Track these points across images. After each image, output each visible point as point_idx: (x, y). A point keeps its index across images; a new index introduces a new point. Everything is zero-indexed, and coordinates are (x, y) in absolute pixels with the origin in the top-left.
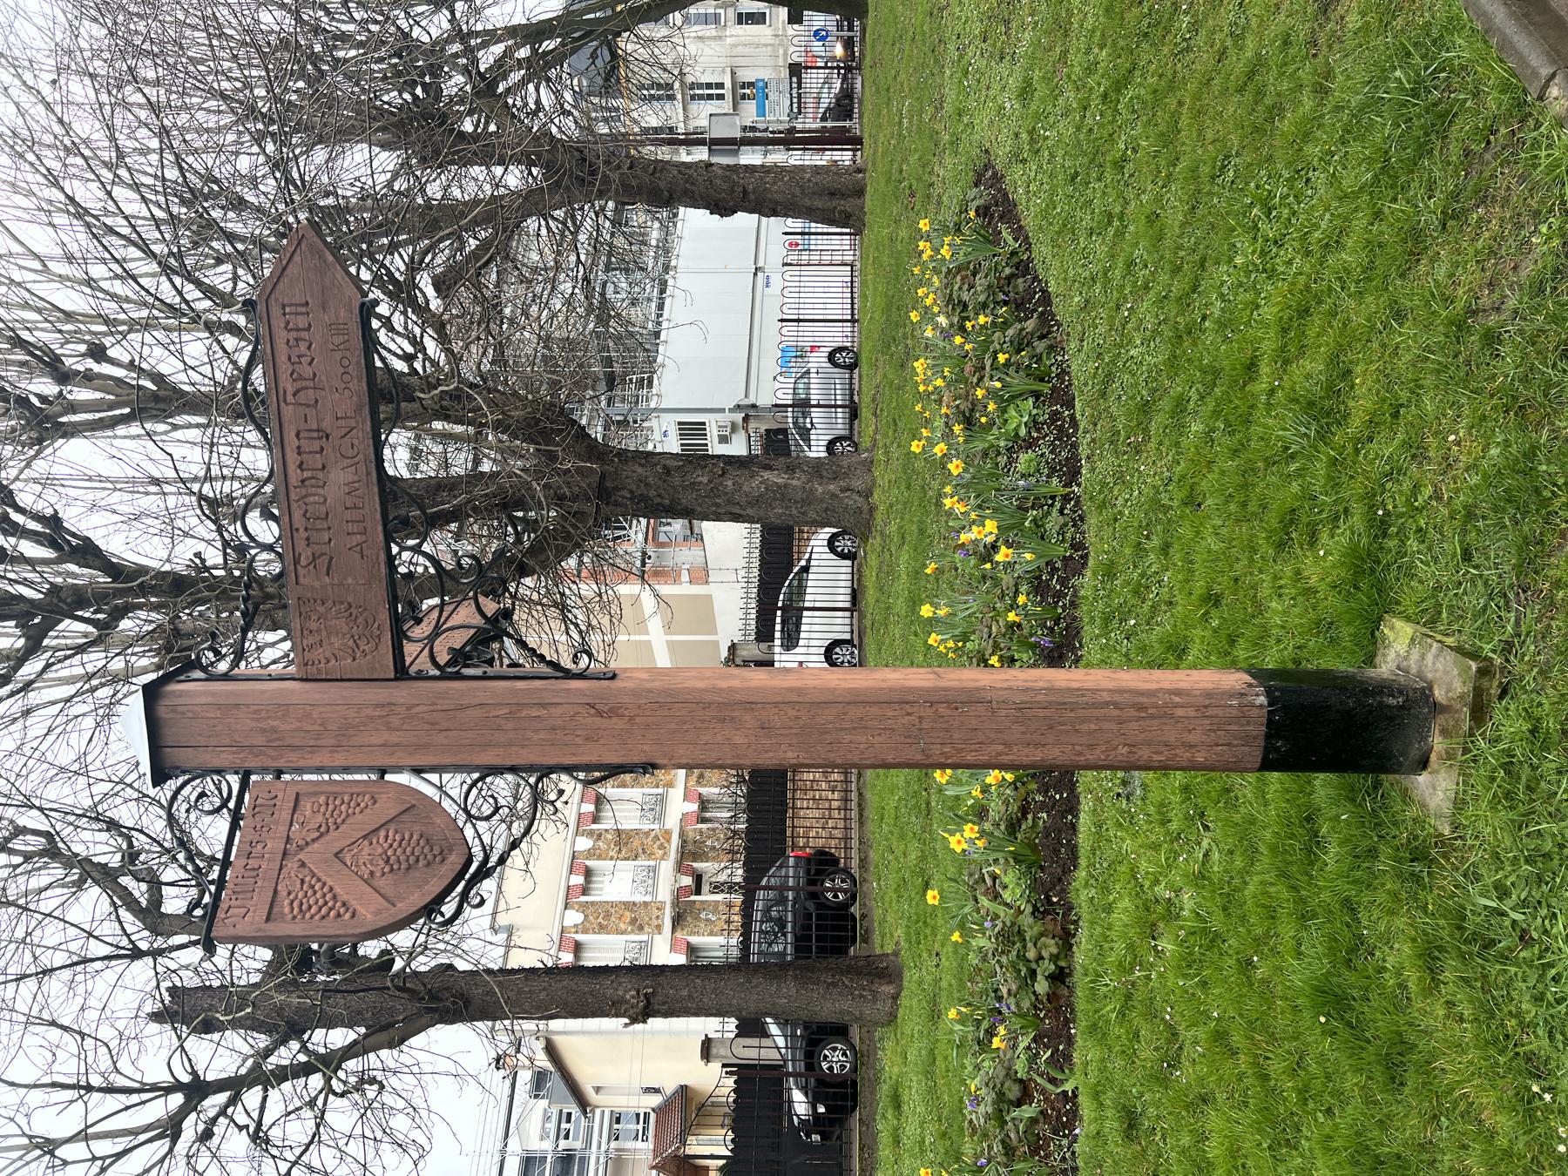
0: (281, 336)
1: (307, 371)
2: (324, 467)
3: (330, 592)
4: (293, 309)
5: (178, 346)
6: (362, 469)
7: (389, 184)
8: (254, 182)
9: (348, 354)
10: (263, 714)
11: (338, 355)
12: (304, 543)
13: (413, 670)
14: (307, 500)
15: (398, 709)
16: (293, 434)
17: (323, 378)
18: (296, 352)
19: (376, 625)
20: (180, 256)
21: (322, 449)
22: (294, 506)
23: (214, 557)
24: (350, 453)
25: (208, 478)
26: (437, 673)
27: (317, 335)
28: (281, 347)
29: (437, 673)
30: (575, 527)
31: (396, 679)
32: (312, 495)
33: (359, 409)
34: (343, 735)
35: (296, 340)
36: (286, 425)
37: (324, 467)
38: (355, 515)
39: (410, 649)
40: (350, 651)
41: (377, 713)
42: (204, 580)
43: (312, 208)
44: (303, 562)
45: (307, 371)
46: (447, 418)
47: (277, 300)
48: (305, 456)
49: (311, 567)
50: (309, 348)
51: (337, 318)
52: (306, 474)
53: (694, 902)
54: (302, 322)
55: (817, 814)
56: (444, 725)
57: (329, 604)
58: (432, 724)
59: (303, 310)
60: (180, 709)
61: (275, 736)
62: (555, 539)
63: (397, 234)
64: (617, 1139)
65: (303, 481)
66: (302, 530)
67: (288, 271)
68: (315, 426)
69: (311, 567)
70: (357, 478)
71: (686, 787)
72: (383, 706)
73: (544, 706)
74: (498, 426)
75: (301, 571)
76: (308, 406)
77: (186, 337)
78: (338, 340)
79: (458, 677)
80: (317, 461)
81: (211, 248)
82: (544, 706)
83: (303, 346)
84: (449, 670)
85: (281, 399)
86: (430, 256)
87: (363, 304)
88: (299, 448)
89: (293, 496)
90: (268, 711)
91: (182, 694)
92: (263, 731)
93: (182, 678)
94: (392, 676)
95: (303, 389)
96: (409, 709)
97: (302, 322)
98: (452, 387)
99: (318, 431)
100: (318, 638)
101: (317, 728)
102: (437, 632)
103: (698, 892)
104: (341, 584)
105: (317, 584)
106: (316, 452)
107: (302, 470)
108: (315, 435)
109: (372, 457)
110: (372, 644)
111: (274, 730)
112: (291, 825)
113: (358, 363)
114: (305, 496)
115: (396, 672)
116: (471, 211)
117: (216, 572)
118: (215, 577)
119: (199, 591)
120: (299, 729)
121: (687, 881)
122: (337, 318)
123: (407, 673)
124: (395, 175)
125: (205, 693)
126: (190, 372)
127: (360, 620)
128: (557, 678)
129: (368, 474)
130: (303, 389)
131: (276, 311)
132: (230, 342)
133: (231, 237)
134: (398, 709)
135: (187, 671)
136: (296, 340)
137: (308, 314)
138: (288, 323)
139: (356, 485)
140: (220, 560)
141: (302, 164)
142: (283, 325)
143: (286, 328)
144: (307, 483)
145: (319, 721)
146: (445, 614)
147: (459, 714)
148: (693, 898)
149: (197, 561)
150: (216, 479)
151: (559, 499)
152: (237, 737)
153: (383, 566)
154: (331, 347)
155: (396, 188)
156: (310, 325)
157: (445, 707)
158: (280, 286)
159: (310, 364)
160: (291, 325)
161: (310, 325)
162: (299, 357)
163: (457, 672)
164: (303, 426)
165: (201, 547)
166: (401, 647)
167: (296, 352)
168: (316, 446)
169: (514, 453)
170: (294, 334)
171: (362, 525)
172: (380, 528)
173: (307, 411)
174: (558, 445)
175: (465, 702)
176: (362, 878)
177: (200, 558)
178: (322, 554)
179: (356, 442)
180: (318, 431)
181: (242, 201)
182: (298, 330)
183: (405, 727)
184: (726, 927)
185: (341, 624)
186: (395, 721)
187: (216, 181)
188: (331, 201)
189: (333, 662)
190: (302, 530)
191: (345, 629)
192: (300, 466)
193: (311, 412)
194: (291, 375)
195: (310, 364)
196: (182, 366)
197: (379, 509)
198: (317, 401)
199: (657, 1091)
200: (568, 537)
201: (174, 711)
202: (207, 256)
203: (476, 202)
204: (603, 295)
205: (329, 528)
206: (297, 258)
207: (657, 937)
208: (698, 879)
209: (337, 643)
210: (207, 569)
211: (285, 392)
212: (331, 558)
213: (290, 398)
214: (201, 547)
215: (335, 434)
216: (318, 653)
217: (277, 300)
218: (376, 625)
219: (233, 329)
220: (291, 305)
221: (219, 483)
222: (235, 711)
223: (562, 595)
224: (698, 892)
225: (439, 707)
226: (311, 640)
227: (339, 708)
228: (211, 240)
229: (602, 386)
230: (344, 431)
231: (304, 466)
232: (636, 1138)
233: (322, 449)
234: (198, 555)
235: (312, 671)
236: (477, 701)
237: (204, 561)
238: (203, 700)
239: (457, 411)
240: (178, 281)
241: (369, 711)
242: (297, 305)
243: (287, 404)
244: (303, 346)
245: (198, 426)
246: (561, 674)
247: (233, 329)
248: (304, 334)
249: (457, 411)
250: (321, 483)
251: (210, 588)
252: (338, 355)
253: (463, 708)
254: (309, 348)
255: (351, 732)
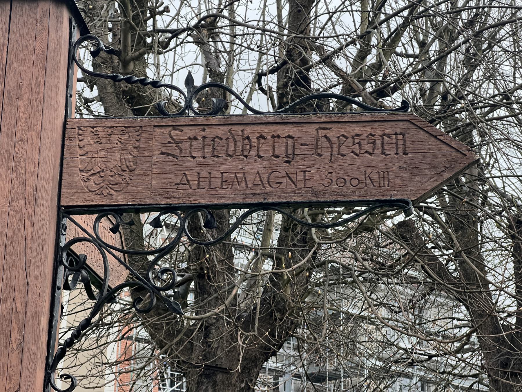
0: (378, 130)
1: (346, 149)
2: (260, 157)
3: (145, 154)
4: (402, 142)
5: (349, 8)
6: (258, 190)
7: (494, 189)
8: (490, 76)
10: (34, 89)
11: (361, 177)
12: (192, 134)
13: (66, 221)
14: (231, 140)
15: (30, 208)
16: (291, 133)
17: (341, 163)
18: (364, 141)
19: (112, 192)
20: (425, 14)
21: (277, 157)
22: (226, 129)
23: (162, 22)
24: (273, 181)
25: (233, 24)
26: (62, 244)
28: (368, 129)
29: (62, 244)
30: (178, 344)
31: (59, 206)
32: (235, 145)
33: (314, 192)
34: (9, 157)
35: (374, 143)
36: (299, 127)
37: (260, 157)
38: (216, 179)
39: (83, 219)
40: (89, 168)
41: (28, 188)
42: (144, 13)
43: (472, 126)
44: (174, 133)
45: (346, 149)
46: (285, 229)
47: (408, 129)
48: (270, 141)
49: (170, 140)
50: (367, 152)
51: (394, 178)
52: (254, 141)
54: (390, 148)
56: (11, 249)
57: (135, 152)
58: (13, 238)
59: (400, 151)
60: (46, 19)
61: (13, 98)
62: (167, 324)
63: (450, 194)
65: (248, 138)
66: (204, 133)
67: (433, 140)
68: (297, 152)
69: (170, 140)
70: (250, 184)
72: (35, 195)
73: (21, 345)
74: (276, 276)
75: (166, 131)
76: (316, 147)
77: (358, 17)
78: (375, 177)
79: (57, 262)
80: (267, 152)
81: (433, 40)
82: (21, 345)
83: (369, 147)
84: (64, 255)
85: (322, 126)
86: (430, 219)
87: (407, 203)
88: (279, 137)
89: (234, 129)
90: (38, 93)
91: (59, 22)
92: (20, 88)
93: (73, 23)
94: (62, 203)
95: (331, 144)
96: (30, 218)
97: (390, 148)
98: (315, 237)
99: (294, 154)
100: (103, 140)
101: (18, 135)
102: (102, 246)
104: (152, 164)
105: (153, 143)
106: (274, 151)
107: (258, 138)
108: (290, 151)
109: (270, 201)
110: (94, 188)
111: (19, 97)
113: (354, 193)
114: (234, 139)
115: (66, 207)
116: (473, 261)
117: (150, 22)
118: (146, 21)
119: (134, 8)
120: (18, 118)
122: (394, 178)
123: (63, 217)
124: (502, 195)
125: (59, 41)
126: (327, 16)
127: (118, 179)
128: (47, 358)
129: (254, 195)
130: (331, 144)
131: (399, 127)
132: (353, 51)
133: (442, 58)
134: (30, 208)
135: (79, 27)
136: (374, 143)
137: (397, 154)
138: (389, 137)
139: (244, 184)
140: (160, 25)
141: (509, 119)
142: (387, 132)
143: (384, 134)
144: (246, 141)
145: (24, 137)
146: (117, 253)
147: (21, 263)
149: (161, 9)
150: (232, 30)
151: (206, 328)
152: (15, 65)
153: (168, 202)
154: (368, 171)
155: (490, 194)
156: (387, 155)
157: (28, 251)
158: (420, 133)
159: (353, 152)
160: (386, 139)
161: (387, 155)
162: (359, 143)
163: (61, 263)
164: (298, 142)
165: (173, 12)
166: (92, 213)
167: (364, 141)
168: (282, 152)
169: (250, 288)
170: (379, 141)
171: (206, 186)
172: (203, 202)
173: (311, 147)
174: (261, 334)
175: (33, 271)
177: (164, 11)
178: (181, 150)
179: (283, 186)
180: (294, 154)
181: (473, 67)
182: (383, 144)
183: (12, 213)
185: (116, 162)
186: (19, 204)
187: (490, 47)
188: (477, 139)
189: (80, 152)
190: (204, 133)
191: (111, 165)
192: (262, 137)
193: (310, 149)
194: (343, 136)
195: (353, 152)
196: (332, 9)
197: (221, 202)
198: (320, 155)
200: (170, 335)
201: (44, 15)
202: (426, 36)
203: (481, 266)
204: (400, 375)
205: (204, 157)
206: (445, 148)
209: (99, 156)
210: (153, 16)
211: (328, 129)
212: (177, 157)
213: (323, 133)
214: (173, 12)
215: (290, 169)
216: (89, 140)
217: (408, 129)
218: (112, 192)
219: (362, 55)
220: (404, 141)
221: (228, 31)
222: (40, 66)
223: (111, 325)
225: (29, 245)
226: (101, 134)
227: (36, 155)
228: (439, 40)
229: (313, 370)
231: (262, 140)
233: (277, 157)
234: (167, 9)
235: (72, 133)
236: (31, 280)
237: (161, 13)
238: (51, 40)
239: (293, 240)
240: (406, 13)
241: (30, 182)
242: (405, 145)
243: (317, 130)
245: (279, 16)
246: (51, 362)
247: (362, 55)
248: (379, 149)
249: (293, 240)
250: (246, 153)
251: (136, 18)
252: (361, 177)
253: (26, 267)
254: (367, 152)
255: (11, 164)
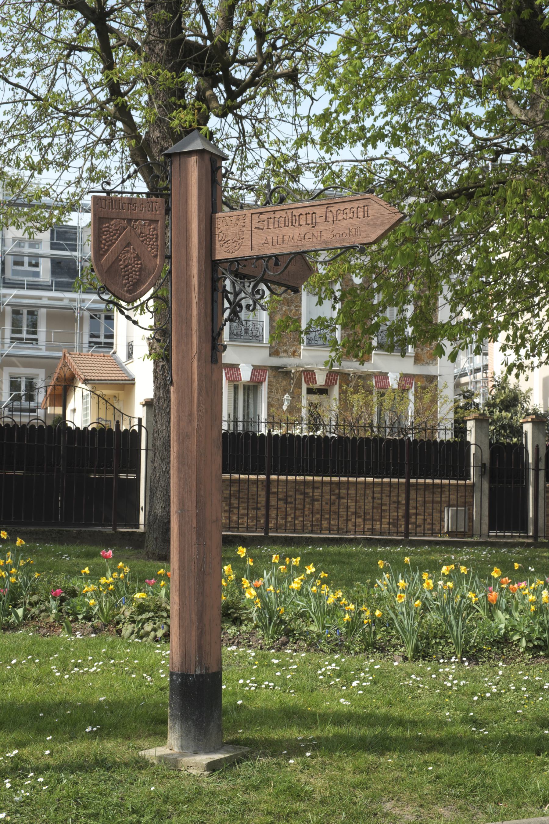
9: (348, 236)
11: (347, 231)
27: (355, 221)
33: (326, 242)
45: (340, 217)
48: (305, 216)
53: (300, 388)
54: (361, 214)
55: (369, 507)
64: (91, 317)
68: (318, 221)
71: (414, 376)
97: (361, 214)
103: (310, 391)
108: (314, 221)
112: (144, 220)
121: (321, 380)
148: (304, 387)
168: (309, 222)
173: (324, 217)
176: (119, 256)
184: (276, 420)
199: (130, 355)
207: (267, 352)
208: (323, 391)
215: (313, 231)
224: (310, 391)
230: (315, 234)
232: (92, 336)
244: (351, 215)
248: (355, 216)
